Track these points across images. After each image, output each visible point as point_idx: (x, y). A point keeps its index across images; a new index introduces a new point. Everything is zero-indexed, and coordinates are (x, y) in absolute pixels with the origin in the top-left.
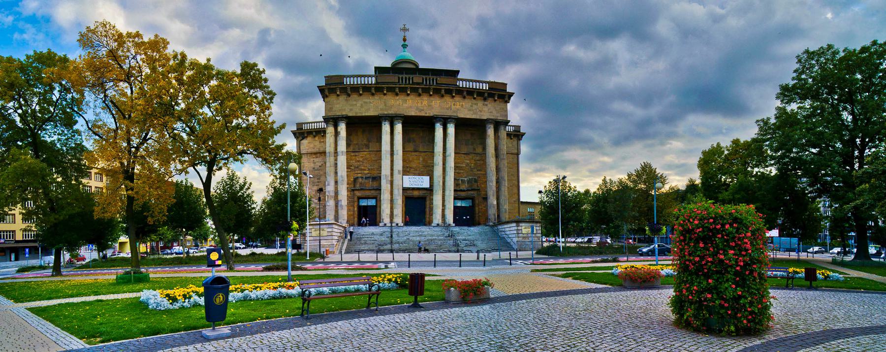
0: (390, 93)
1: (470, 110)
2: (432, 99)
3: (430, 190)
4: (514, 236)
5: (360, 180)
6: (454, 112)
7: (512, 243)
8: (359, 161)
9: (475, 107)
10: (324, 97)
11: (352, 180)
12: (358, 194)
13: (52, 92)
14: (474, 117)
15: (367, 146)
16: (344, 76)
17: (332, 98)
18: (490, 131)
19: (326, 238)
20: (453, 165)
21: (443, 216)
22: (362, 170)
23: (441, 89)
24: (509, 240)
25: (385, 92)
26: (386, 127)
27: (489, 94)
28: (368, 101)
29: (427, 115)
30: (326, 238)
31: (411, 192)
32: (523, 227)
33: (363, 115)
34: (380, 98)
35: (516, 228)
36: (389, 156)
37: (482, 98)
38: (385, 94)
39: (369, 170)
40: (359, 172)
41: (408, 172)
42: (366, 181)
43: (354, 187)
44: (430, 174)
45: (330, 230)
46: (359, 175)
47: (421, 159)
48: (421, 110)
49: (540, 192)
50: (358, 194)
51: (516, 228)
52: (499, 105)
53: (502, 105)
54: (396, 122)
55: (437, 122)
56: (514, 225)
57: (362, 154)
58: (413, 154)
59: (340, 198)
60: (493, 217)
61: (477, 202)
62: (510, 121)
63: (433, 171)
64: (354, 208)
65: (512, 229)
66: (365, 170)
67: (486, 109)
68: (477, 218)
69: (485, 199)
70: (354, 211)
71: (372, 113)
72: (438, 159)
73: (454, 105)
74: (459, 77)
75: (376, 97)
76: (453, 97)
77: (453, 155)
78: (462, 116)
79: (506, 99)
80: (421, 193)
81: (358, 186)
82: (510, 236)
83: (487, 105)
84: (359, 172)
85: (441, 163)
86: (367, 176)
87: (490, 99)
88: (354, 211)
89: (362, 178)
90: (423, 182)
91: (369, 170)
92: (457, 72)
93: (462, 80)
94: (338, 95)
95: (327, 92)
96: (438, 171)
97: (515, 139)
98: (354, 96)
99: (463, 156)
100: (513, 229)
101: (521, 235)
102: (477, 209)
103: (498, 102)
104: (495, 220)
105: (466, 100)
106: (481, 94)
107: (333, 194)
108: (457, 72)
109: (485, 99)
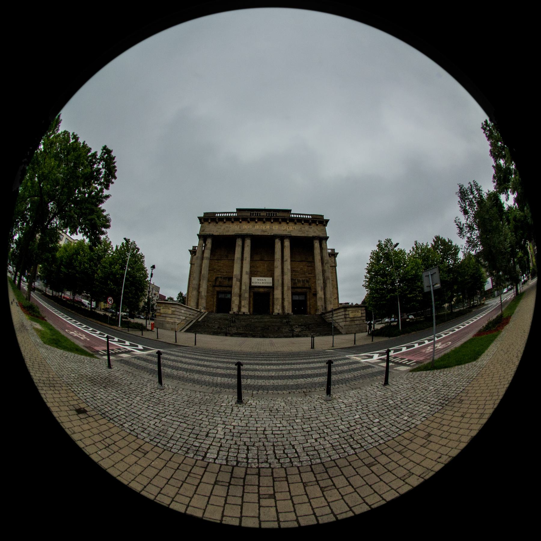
0: (244, 222)
1: (299, 231)
2: (272, 225)
3: (272, 288)
4: (341, 320)
5: (220, 279)
6: (289, 232)
7: (339, 328)
8: (220, 266)
9: (303, 229)
10: (201, 223)
11: (214, 279)
12: (218, 289)
13: (68, 242)
14: (303, 235)
15: (227, 256)
16: (216, 213)
17: (206, 224)
18: (317, 244)
19: (171, 316)
20: (289, 267)
21: (283, 307)
22: (221, 272)
23: (279, 219)
24: (336, 325)
25: (241, 221)
26: (239, 242)
27: (312, 220)
28: (229, 226)
29: (269, 234)
30: (171, 316)
31: (257, 289)
32: (350, 312)
33: (225, 234)
34: (237, 225)
35: (344, 313)
36: (239, 262)
37: (308, 224)
38: (240, 222)
39: (227, 272)
40: (219, 273)
41: (256, 274)
42: (224, 280)
43: (215, 283)
44: (272, 276)
45: (173, 309)
46: (219, 276)
47: (266, 265)
48: (264, 231)
49: (367, 264)
50: (218, 289)
51: (344, 313)
52: (320, 227)
53: (322, 227)
54: (246, 239)
55: (276, 238)
56: (343, 310)
57: (222, 262)
58: (260, 262)
59: (201, 289)
60: (320, 307)
61: (308, 297)
62: (328, 237)
63: (274, 274)
64: (214, 299)
65: (339, 314)
66: (223, 272)
67: (311, 230)
68: (308, 310)
69: (315, 295)
70: (214, 302)
71: (231, 233)
72: (278, 263)
73: (288, 228)
74: (292, 212)
75: (235, 224)
76: (288, 223)
77: (289, 260)
78: (294, 235)
79: (324, 223)
80: (266, 290)
81: (218, 283)
82: (337, 321)
83: (311, 228)
84: (219, 273)
85: (280, 267)
86: (225, 277)
87: (314, 224)
88: (214, 302)
89: (221, 277)
90: (266, 281)
91: (227, 272)
92: (290, 211)
93: (294, 214)
94: (209, 223)
95: (203, 221)
96: (277, 272)
97: (333, 257)
98: (221, 223)
99: (297, 262)
100: (341, 314)
101: (348, 319)
102: (308, 302)
103: (319, 226)
104: (323, 310)
105: (297, 225)
106: (306, 221)
107: (197, 287)
108: (290, 211)
109: (310, 224)
